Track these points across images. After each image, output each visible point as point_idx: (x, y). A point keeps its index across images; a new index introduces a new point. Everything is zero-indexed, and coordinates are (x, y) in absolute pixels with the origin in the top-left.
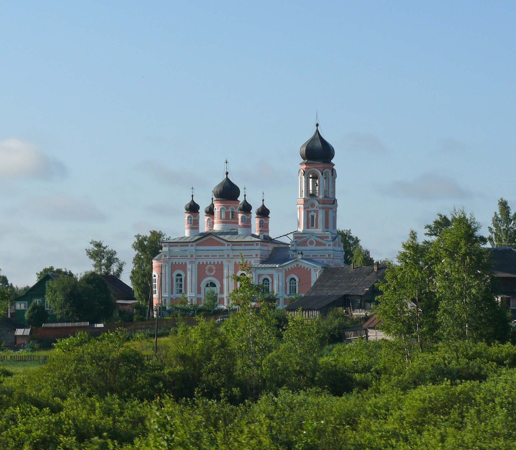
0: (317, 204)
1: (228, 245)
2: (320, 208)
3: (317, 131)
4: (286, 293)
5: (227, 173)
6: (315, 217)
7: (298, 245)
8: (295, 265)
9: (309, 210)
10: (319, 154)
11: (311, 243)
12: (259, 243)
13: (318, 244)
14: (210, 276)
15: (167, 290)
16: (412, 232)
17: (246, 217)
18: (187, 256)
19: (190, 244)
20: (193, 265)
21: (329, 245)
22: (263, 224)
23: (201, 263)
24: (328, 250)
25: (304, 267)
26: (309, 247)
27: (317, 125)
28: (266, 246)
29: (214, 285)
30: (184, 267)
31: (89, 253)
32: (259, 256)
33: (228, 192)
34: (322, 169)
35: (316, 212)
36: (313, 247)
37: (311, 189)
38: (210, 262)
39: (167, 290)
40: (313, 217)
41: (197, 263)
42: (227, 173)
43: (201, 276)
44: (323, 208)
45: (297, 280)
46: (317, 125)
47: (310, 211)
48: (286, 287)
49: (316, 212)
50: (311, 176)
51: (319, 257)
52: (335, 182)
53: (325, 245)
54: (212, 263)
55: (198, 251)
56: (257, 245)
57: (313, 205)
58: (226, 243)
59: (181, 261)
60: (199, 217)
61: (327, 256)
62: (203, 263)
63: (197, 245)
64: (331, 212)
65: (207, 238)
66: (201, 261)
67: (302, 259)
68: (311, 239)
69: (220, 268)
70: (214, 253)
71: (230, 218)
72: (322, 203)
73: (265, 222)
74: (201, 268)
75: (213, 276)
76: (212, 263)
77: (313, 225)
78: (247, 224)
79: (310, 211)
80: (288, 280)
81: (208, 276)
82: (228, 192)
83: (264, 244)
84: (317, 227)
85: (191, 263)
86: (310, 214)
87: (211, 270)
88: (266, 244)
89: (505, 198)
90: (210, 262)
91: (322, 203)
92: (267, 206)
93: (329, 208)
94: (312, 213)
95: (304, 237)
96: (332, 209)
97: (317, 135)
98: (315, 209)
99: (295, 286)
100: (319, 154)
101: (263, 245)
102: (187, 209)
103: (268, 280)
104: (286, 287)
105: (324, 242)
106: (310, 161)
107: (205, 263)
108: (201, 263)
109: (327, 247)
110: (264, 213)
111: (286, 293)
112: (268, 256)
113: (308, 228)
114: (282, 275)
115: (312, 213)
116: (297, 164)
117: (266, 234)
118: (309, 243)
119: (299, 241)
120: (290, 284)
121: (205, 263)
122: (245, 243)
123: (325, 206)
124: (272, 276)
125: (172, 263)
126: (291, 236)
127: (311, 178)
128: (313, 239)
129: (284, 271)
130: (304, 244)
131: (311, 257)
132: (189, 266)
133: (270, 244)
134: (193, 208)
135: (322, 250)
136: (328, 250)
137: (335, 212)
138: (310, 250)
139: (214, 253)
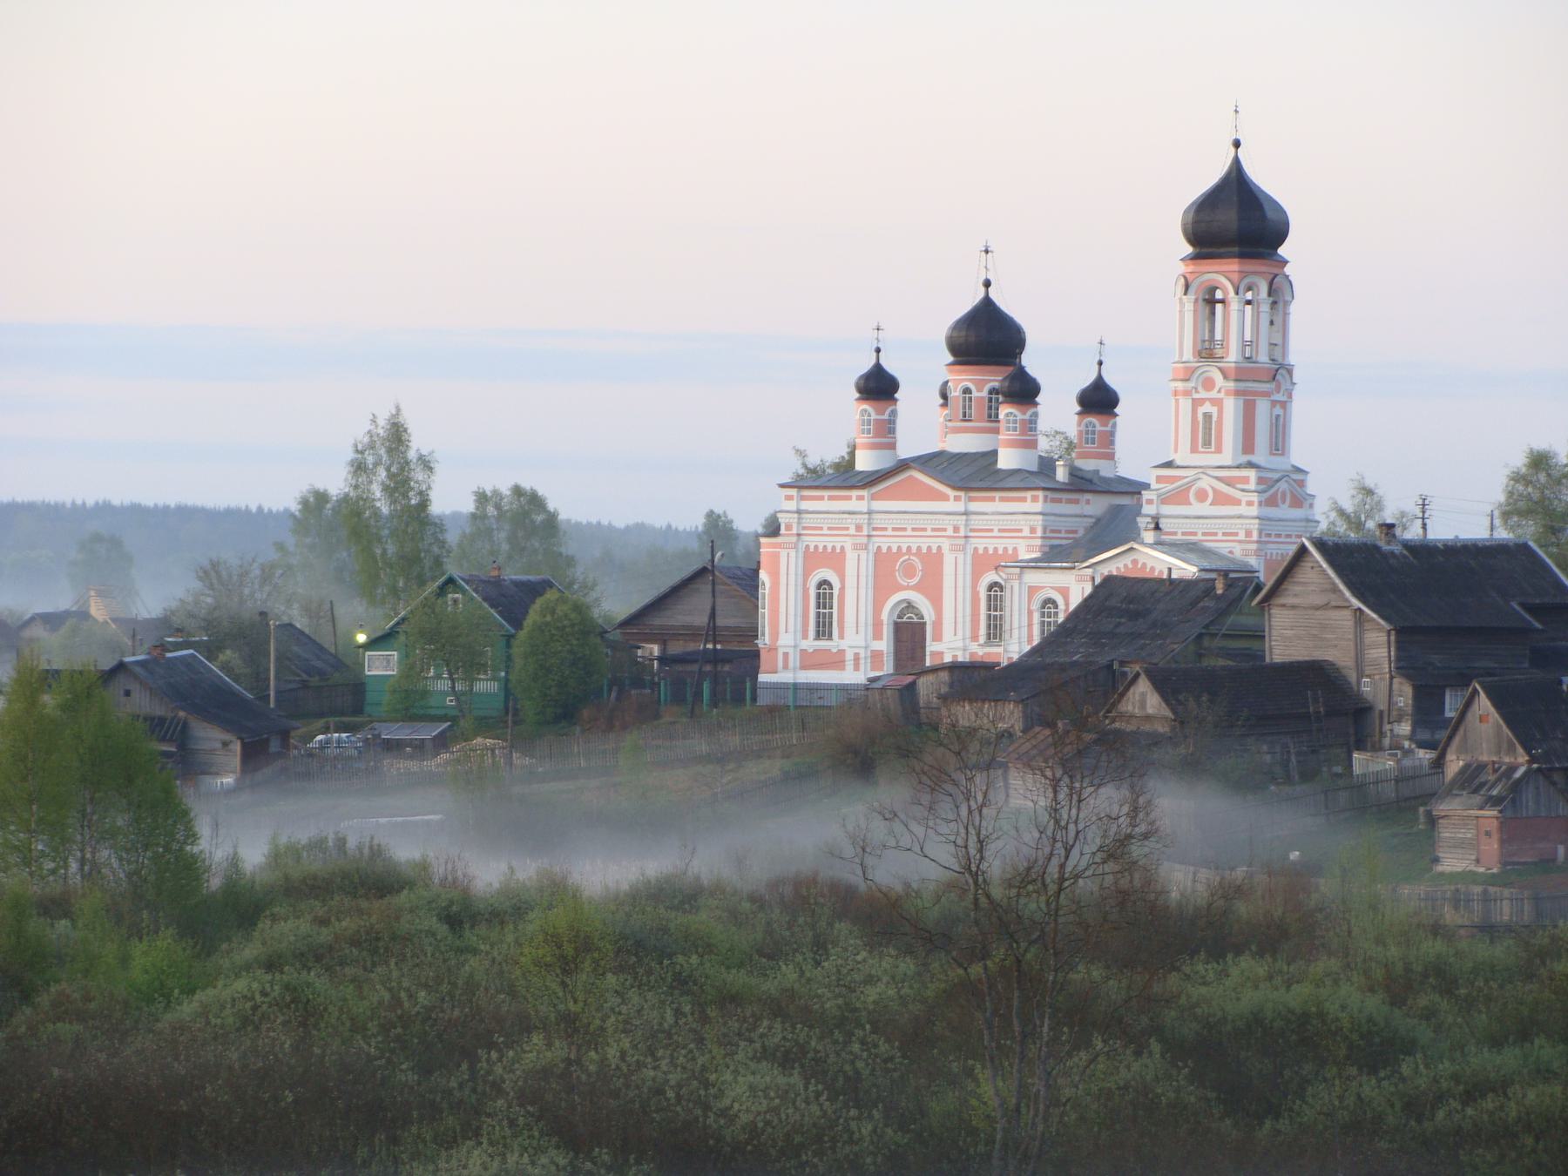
1: (957, 499)
5: (987, 284)
6: (1215, 418)
9: (1196, 396)
10: (1237, 226)
11: (1201, 496)
13: (1220, 499)
14: (908, 588)
15: (791, 629)
18: (1020, 531)
21: (1250, 504)
23: (884, 550)
26: (1196, 508)
27: (1237, 144)
28: (1077, 502)
30: (835, 559)
32: (1039, 533)
34: (1235, 277)
35: (1218, 403)
38: (909, 548)
39: (791, 629)
43: (883, 584)
44: (1237, 393)
47: (1202, 401)
48: (1030, 625)
49: (1218, 403)
51: (1220, 537)
53: (1237, 502)
57: (1209, 384)
59: (1000, 544)
62: (996, 549)
66: (883, 543)
69: (933, 561)
70: (920, 521)
73: (1099, 428)
74: (884, 562)
75: (916, 588)
77: (1207, 443)
79: (1202, 401)
80: (1036, 605)
84: (1219, 450)
85: (856, 547)
87: (909, 571)
90: (909, 548)
92: (1111, 380)
94: (1207, 408)
98: (1213, 394)
99: (831, 614)
101: (1054, 501)
103: (1054, 603)
104: (1030, 625)
105: (1237, 494)
106: (1205, 250)
107: (895, 550)
108: (884, 550)
109: (1243, 509)
111: (975, 638)
112: (1081, 533)
115: (1207, 408)
121: (895, 550)
123: (1242, 385)
125: (976, 549)
128: (1205, 483)
131: (1200, 537)
132: (851, 557)
134: (878, 387)
135: (1187, 517)
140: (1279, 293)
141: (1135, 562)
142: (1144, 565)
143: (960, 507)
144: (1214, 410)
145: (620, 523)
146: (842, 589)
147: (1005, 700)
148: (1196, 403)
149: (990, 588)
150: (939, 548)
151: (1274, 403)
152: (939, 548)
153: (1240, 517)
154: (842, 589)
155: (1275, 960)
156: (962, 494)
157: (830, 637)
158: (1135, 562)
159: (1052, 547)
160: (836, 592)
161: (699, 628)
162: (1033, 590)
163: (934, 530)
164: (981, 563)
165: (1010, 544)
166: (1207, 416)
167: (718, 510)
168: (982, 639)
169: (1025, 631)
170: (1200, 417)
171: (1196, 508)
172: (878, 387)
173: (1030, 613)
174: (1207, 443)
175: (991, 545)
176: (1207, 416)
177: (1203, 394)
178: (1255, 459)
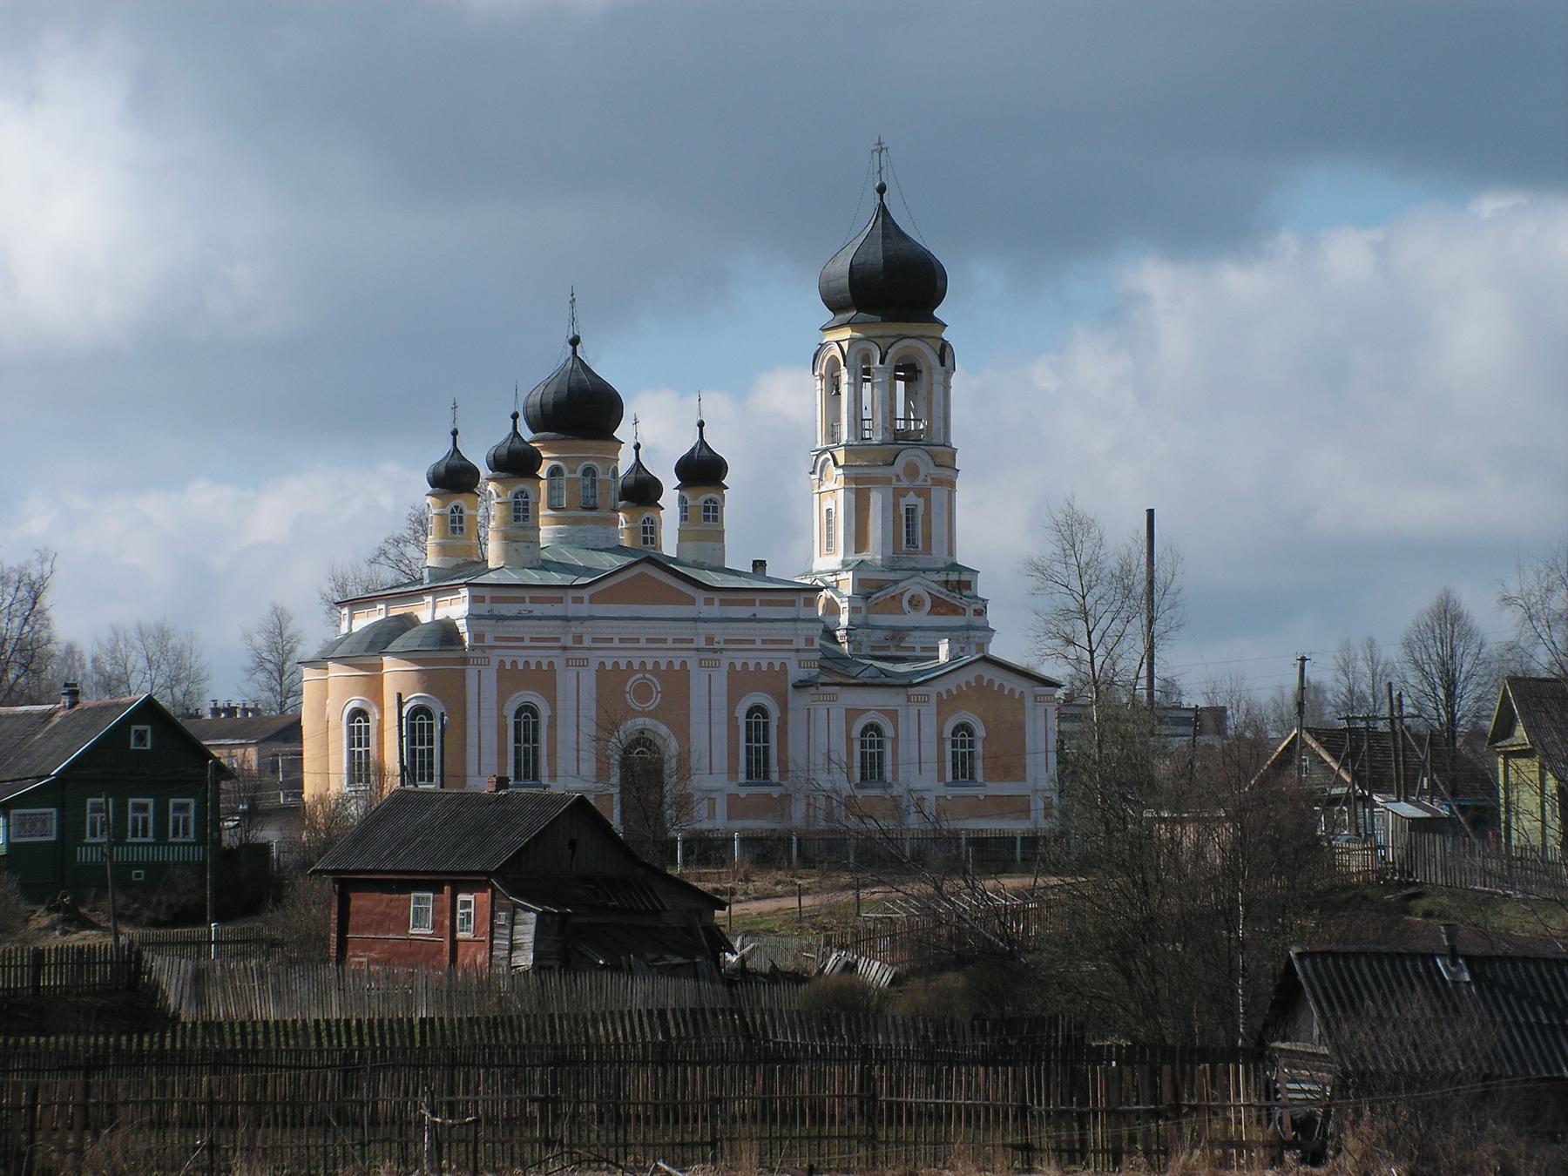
1: (709, 602)
3: (883, 211)
4: (941, 778)
6: (920, 511)
11: (915, 603)
16: (276, 609)
19: (572, 593)
20: (584, 673)
23: (609, 667)
24: (706, 620)
27: (882, 189)
30: (545, 680)
31: (324, 596)
35: (924, 493)
37: (900, 413)
40: (910, 511)
41: (594, 665)
45: (980, 732)
53: (692, 601)
54: (650, 667)
55: (800, 625)
59: (764, 659)
69: (676, 684)
76: (650, 667)
81: (636, 714)
86: (903, 503)
94: (911, 499)
99: (881, 755)
102: (835, 306)
108: (609, 667)
114: (929, 712)
118: (910, 602)
120: (954, 745)
122: (765, 596)
124: (893, 715)
132: (566, 679)
136: (706, 620)
139: (630, 629)
144: (920, 502)
146: (553, 719)
148: (899, 493)
149: (749, 714)
150: (783, 665)
152: (783, 665)
154: (553, 719)
157: (1023, 779)
160: (373, 724)
161: (462, 777)
162: (852, 714)
163: (675, 641)
164: (739, 682)
165: (777, 659)
166: (910, 511)
168: (742, 777)
169: (902, 756)
173: (849, 740)
175: (752, 659)
177: (905, 483)
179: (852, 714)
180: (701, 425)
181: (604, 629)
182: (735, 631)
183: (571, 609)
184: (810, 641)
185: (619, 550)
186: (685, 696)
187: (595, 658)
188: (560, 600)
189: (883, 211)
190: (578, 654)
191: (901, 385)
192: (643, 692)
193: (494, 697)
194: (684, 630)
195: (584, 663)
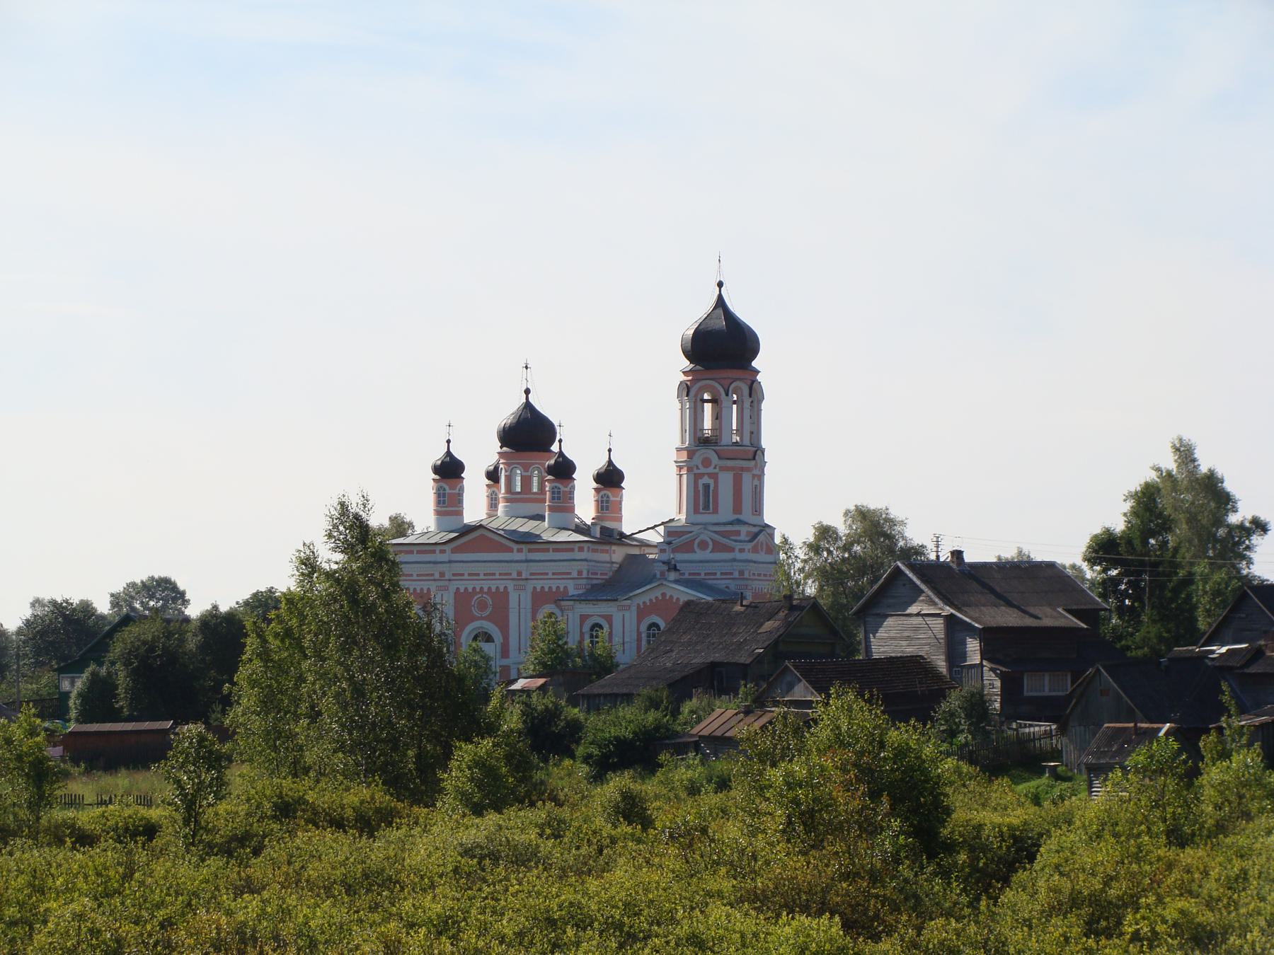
0: (715, 460)
1: (520, 551)
2: (723, 469)
5: (527, 392)
6: (712, 488)
7: (674, 551)
8: (658, 593)
10: (722, 351)
11: (703, 545)
12: (586, 546)
13: (718, 547)
14: (481, 618)
17: (563, 489)
19: (438, 548)
21: (742, 551)
22: (607, 502)
25: (671, 597)
26: (699, 555)
27: (720, 285)
28: (607, 551)
29: (489, 638)
33: (528, 434)
35: (714, 476)
36: (707, 555)
41: (530, 589)
42: (527, 392)
46: (720, 285)
50: (706, 396)
51: (718, 576)
52: (759, 410)
53: (732, 550)
55: (453, 565)
56: (581, 549)
57: (706, 462)
58: (516, 547)
60: (462, 489)
61: (736, 575)
63: (454, 551)
64: (746, 478)
65: (471, 538)
67: (676, 581)
68: (702, 537)
69: (501, 598)
71: (535, 490)
72: (724, 462)
77: (706, 507)
78: (563, 503)
80: (643, 628)
81: (474, 619)
82: (528, 434)
83: (596, 547)
84: (716, 511)
85: (517, 588)
86: (701, 482)
87: (482, 606)
88: (607, 547)
89: (1190, 436)
91: (724, 462)
93: (742, 469)
94: (706, 480)
95: (715, 532)
96: (748, 469)
97: (720, 311)
98: (711, 470)
100: (722, 351)
103: (601, 627)
110: (610, 478)
113: (696, 511)
114: (630, 617)
116: (428, 480)
117: (609, 524)
118: (699, 545)
119: (677, 541)
124: (609, 619)
126: (661, 529)
127: (707, 401)
129: (634, 609)
130: (688, 547)
131: (703, 576)
133: (614, 548)
134: (449, 470)
137: (760, 477)
138: (701, 562)
140: (754, 393)
141: (664, 595)
142: (671, 597)
143: (521, 556)
144: (711, 482)
145: (872, 507)
147: (197, 647)
151: (754, 476)
153: (734, 560)
155: (443, 780)
156: (523, 546)
158: (664, 595)
159: (593, 586)
162: (583, 618)
164: (539, 598)
165: (562, 584)
166: (707, 487)
167: (873, 504)
170: (701, 488)
171: (699, 555)
172: (449, 470)
174: (706, 507)
175: (547, 584)
176: (707, 487)
177: (702, 470)
178: (741, 517)
179: (583, 618)
180: (610, 450)
181: (458, 568)
182: (535, 568)
183: (439, 557)
184: (580, 573)
185: (581, 529)
186: (505, 607)
187: (453, 587)
188: (434, 552)
189: (720, 298)
190: (442, 583)
191: (708, 407)
192: (482, 606)
193: (529, 606)
194: (504, 568)
195: (446, 588)
